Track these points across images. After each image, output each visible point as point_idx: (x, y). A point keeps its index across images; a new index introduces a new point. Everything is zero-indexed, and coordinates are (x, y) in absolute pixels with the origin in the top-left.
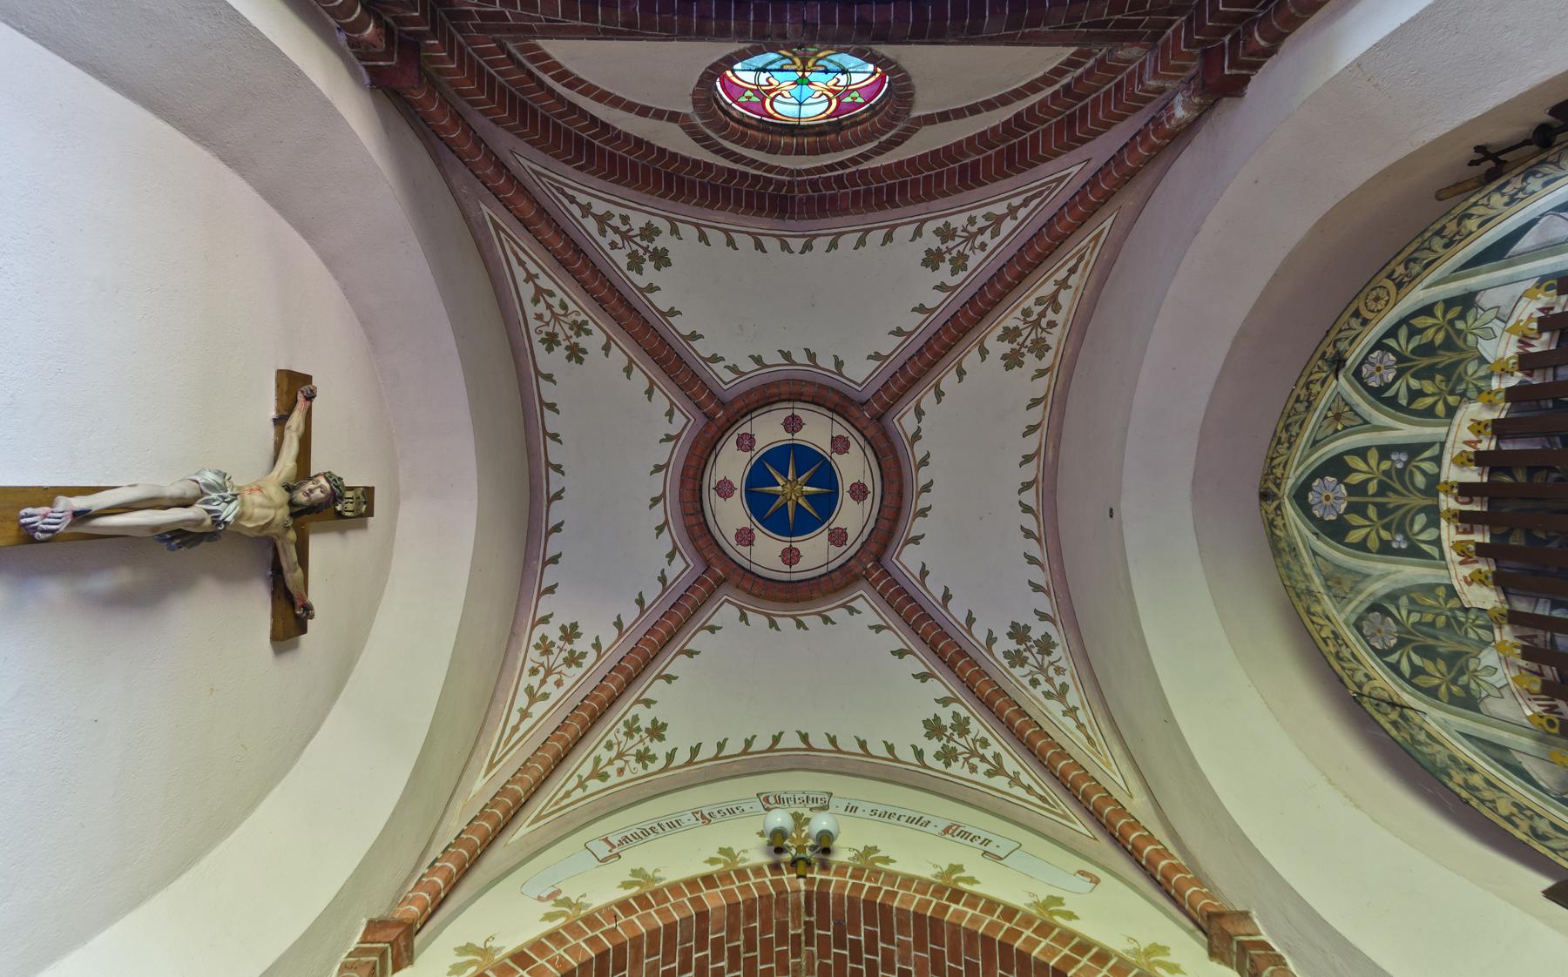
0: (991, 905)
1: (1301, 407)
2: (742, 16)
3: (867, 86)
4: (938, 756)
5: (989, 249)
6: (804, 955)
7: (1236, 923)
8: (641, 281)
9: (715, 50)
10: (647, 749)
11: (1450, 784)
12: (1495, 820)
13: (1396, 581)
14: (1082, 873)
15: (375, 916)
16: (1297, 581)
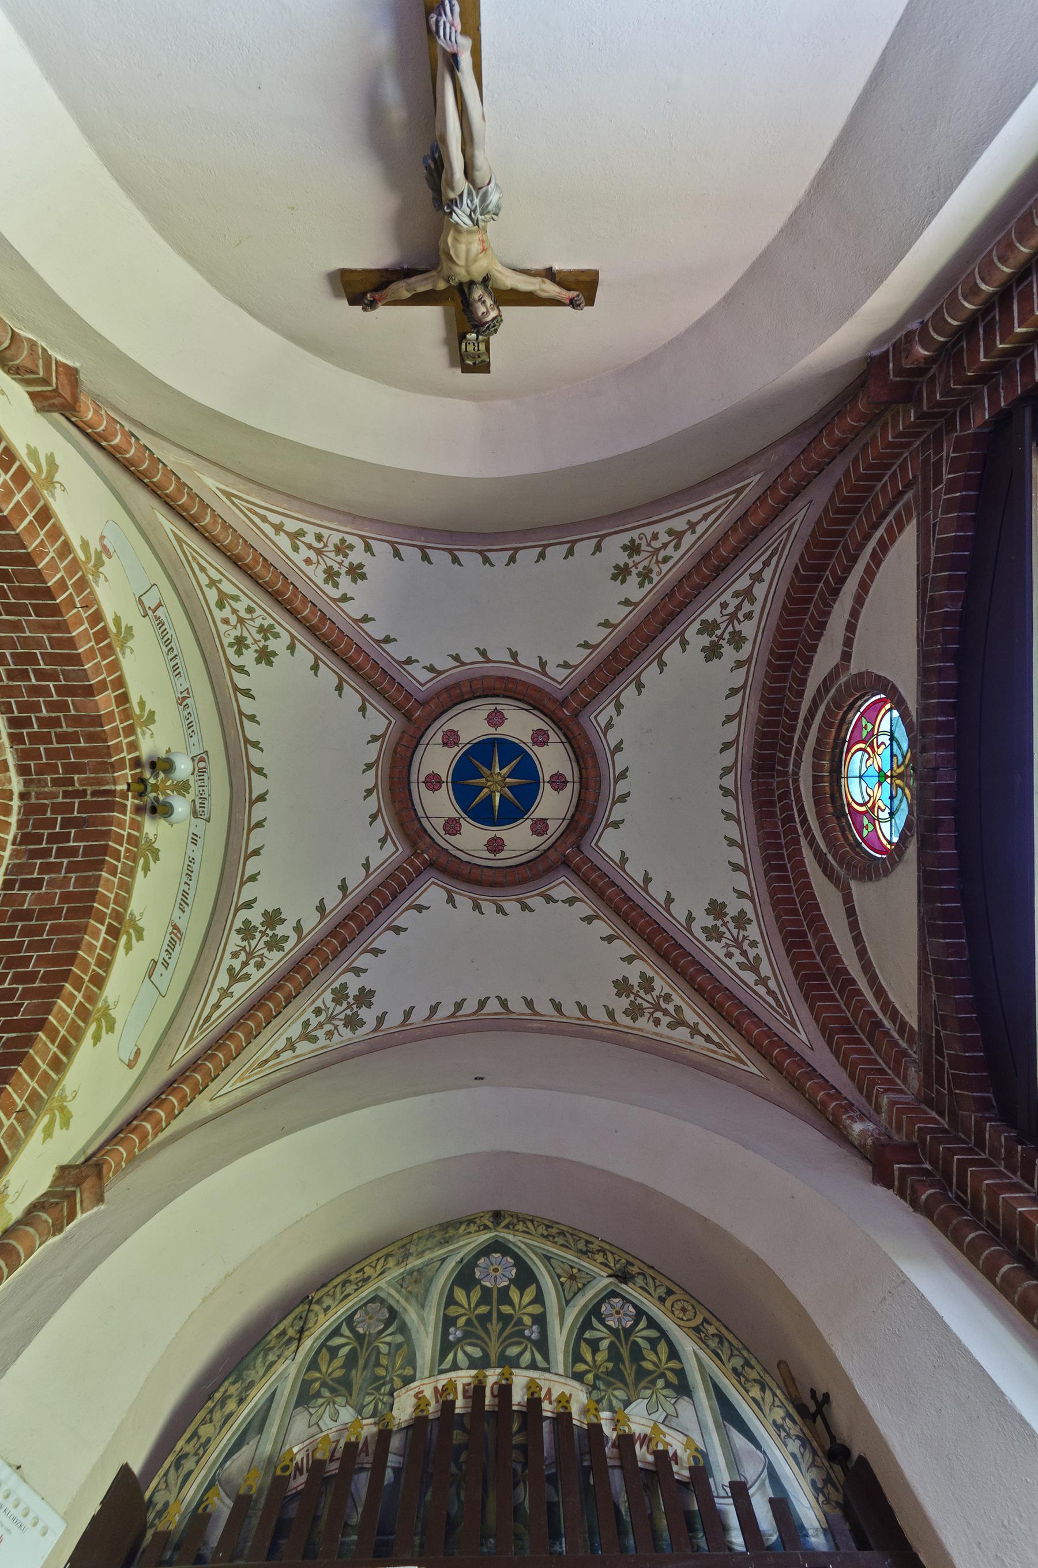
0: (106, 964)
1: (581, 1245)
2: (942, 709)
3: (879, 838)
4: (247, 922)
5: (727, 961)
6: (54, 789)
7: (92, 1190)
8: (691, 634)
9: (909, 691)
10: (247, 647)
11: (226, 1384)
12: (193, 1424)
13: (418, 1332)
14: (138, 1053)
15: (82, 376)
16: (417, 1245)
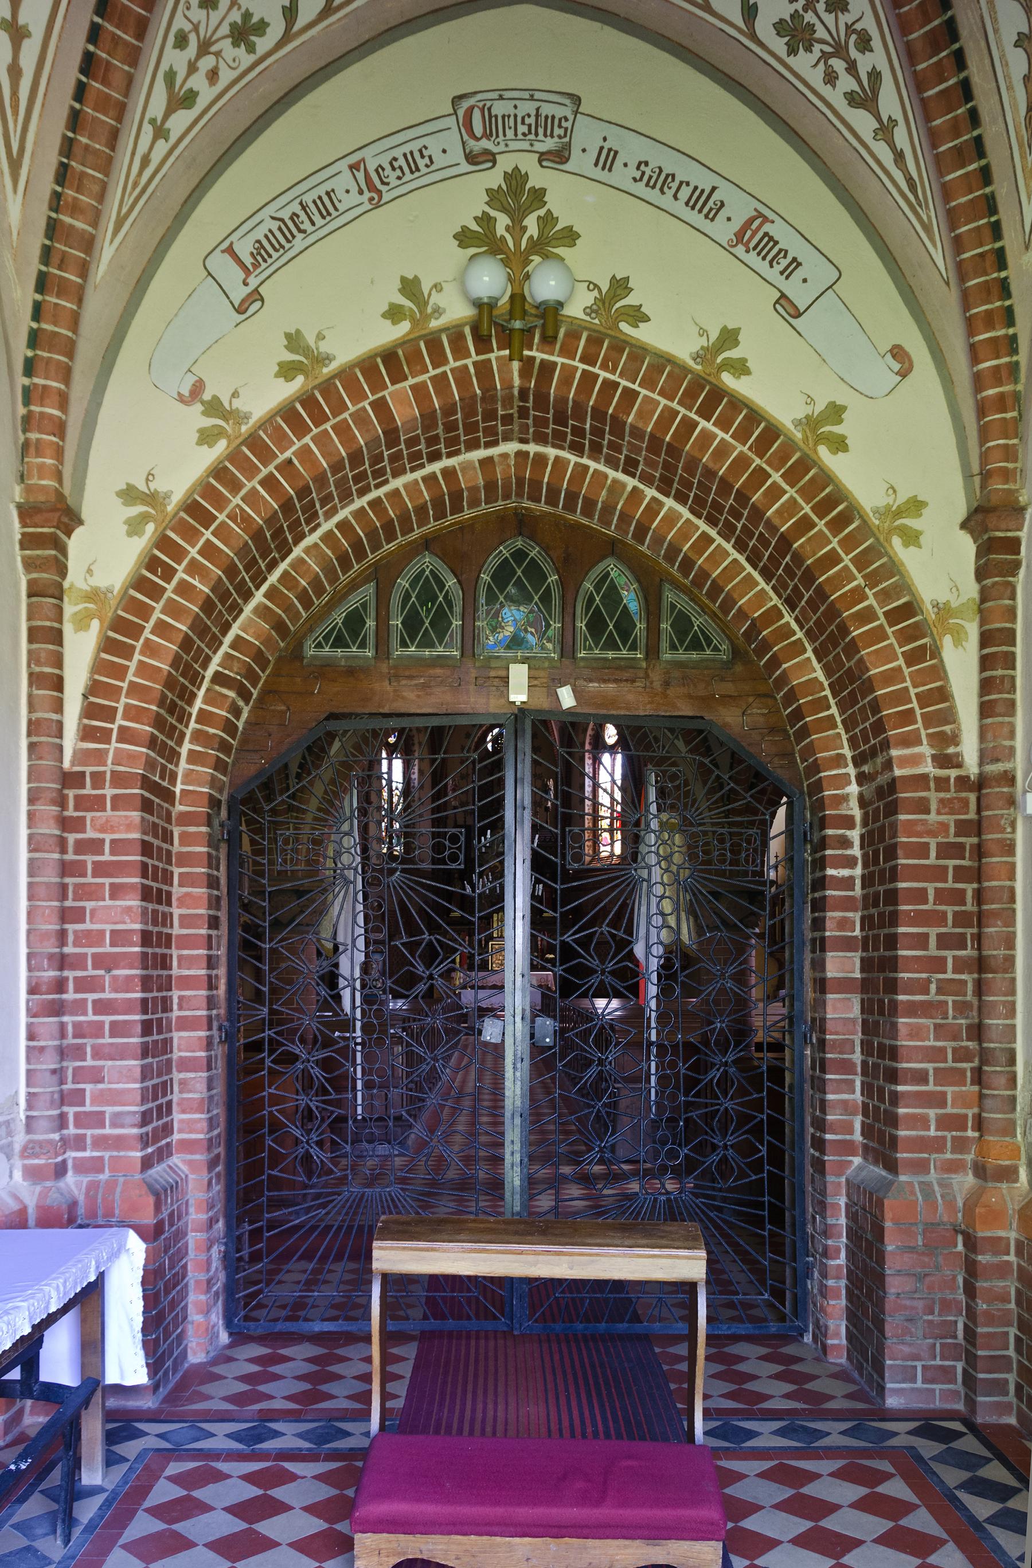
4: (780, 27)
